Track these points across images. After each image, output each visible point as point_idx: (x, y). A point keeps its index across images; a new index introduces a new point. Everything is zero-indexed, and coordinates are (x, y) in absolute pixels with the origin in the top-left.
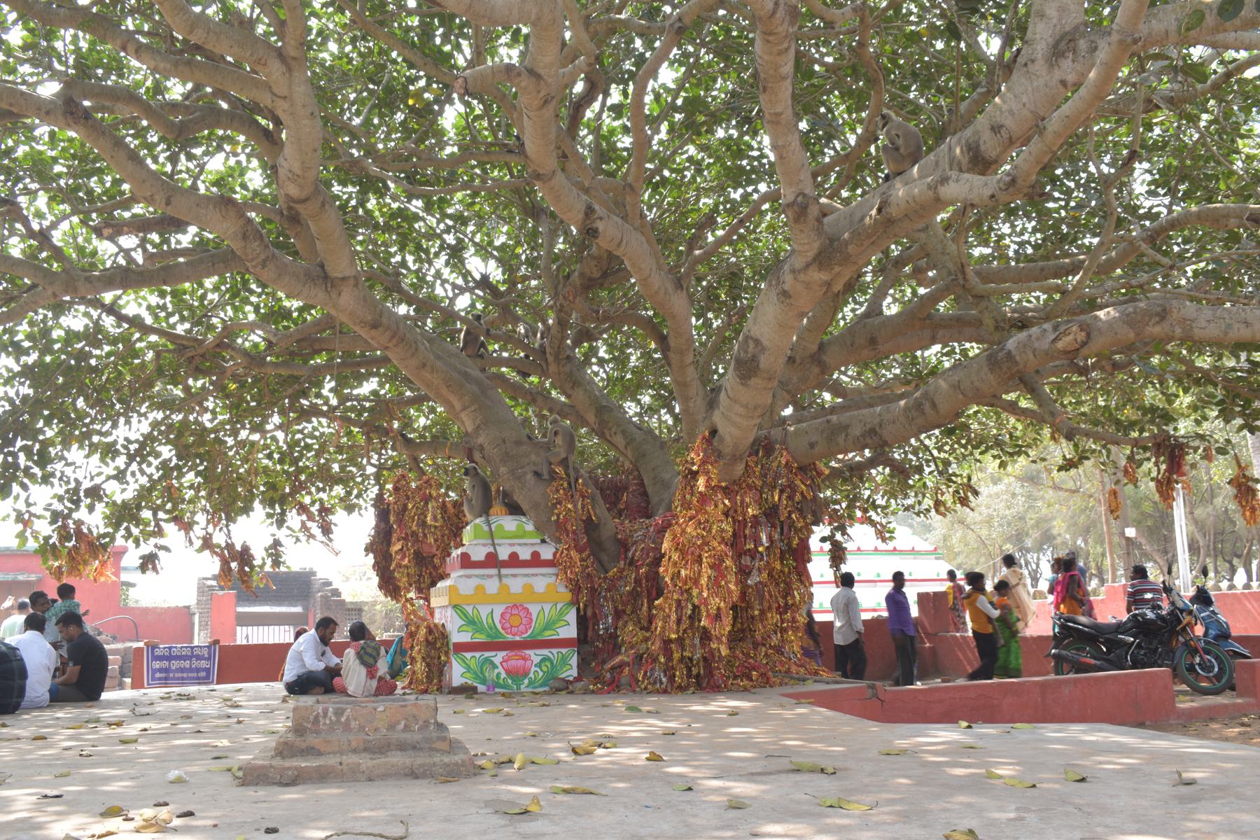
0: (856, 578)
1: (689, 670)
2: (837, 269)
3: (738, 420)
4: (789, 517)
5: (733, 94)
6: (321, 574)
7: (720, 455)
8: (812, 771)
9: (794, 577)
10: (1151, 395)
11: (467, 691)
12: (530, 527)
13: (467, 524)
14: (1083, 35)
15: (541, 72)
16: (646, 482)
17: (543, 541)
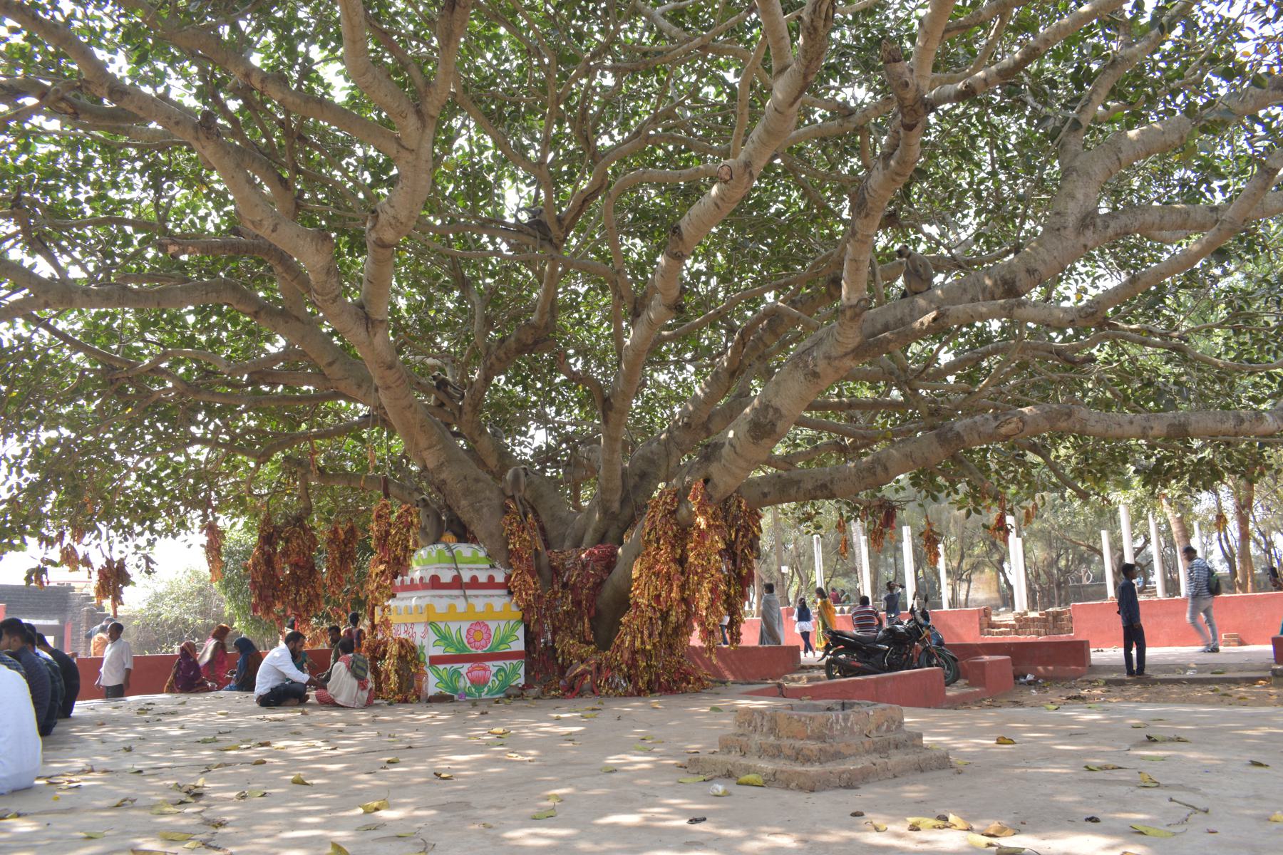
11: (440, 699)
12: (482, 554)
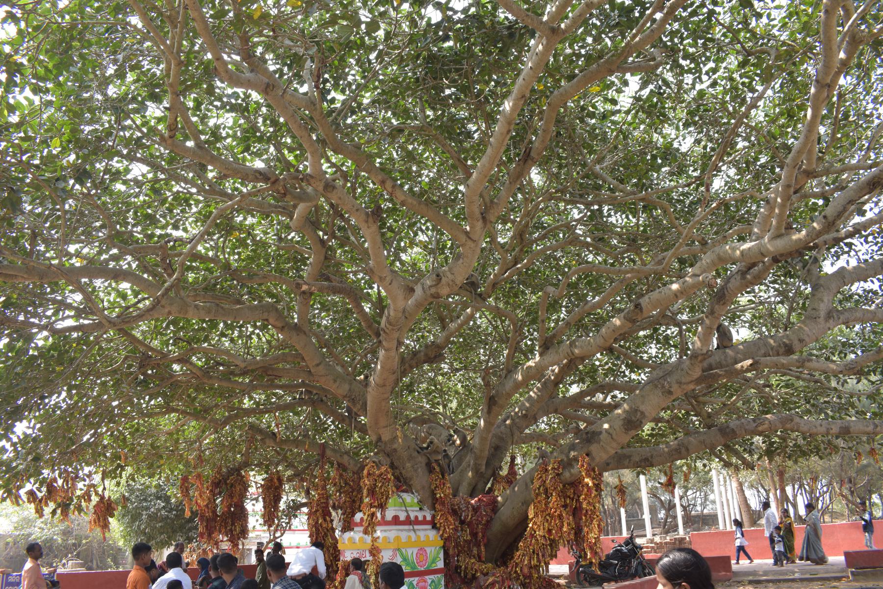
0: (406, 569)
12: (416, 501)
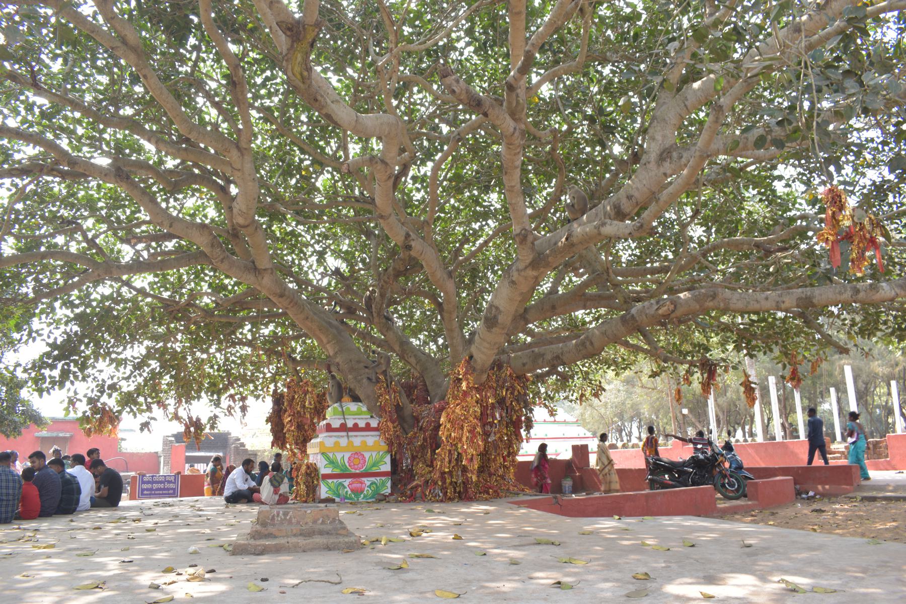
1: (455, 489)
2: (542, 269)
3: (485, 350)
4: (511, 404)
5: (477, 172)
6: (234, 434)
7: (474, 370)
8: (547, 543)
9: (513, 437)
10: (698, 336)
12: (365, 409)
13: (328, 407)
14: (675, 150)
15: (388, 161)
16: (427, 383)
17: (372, 417)
